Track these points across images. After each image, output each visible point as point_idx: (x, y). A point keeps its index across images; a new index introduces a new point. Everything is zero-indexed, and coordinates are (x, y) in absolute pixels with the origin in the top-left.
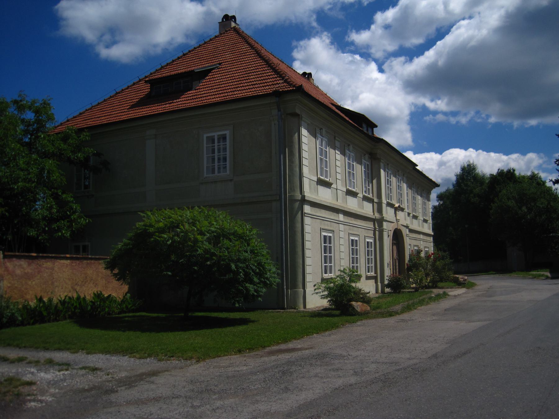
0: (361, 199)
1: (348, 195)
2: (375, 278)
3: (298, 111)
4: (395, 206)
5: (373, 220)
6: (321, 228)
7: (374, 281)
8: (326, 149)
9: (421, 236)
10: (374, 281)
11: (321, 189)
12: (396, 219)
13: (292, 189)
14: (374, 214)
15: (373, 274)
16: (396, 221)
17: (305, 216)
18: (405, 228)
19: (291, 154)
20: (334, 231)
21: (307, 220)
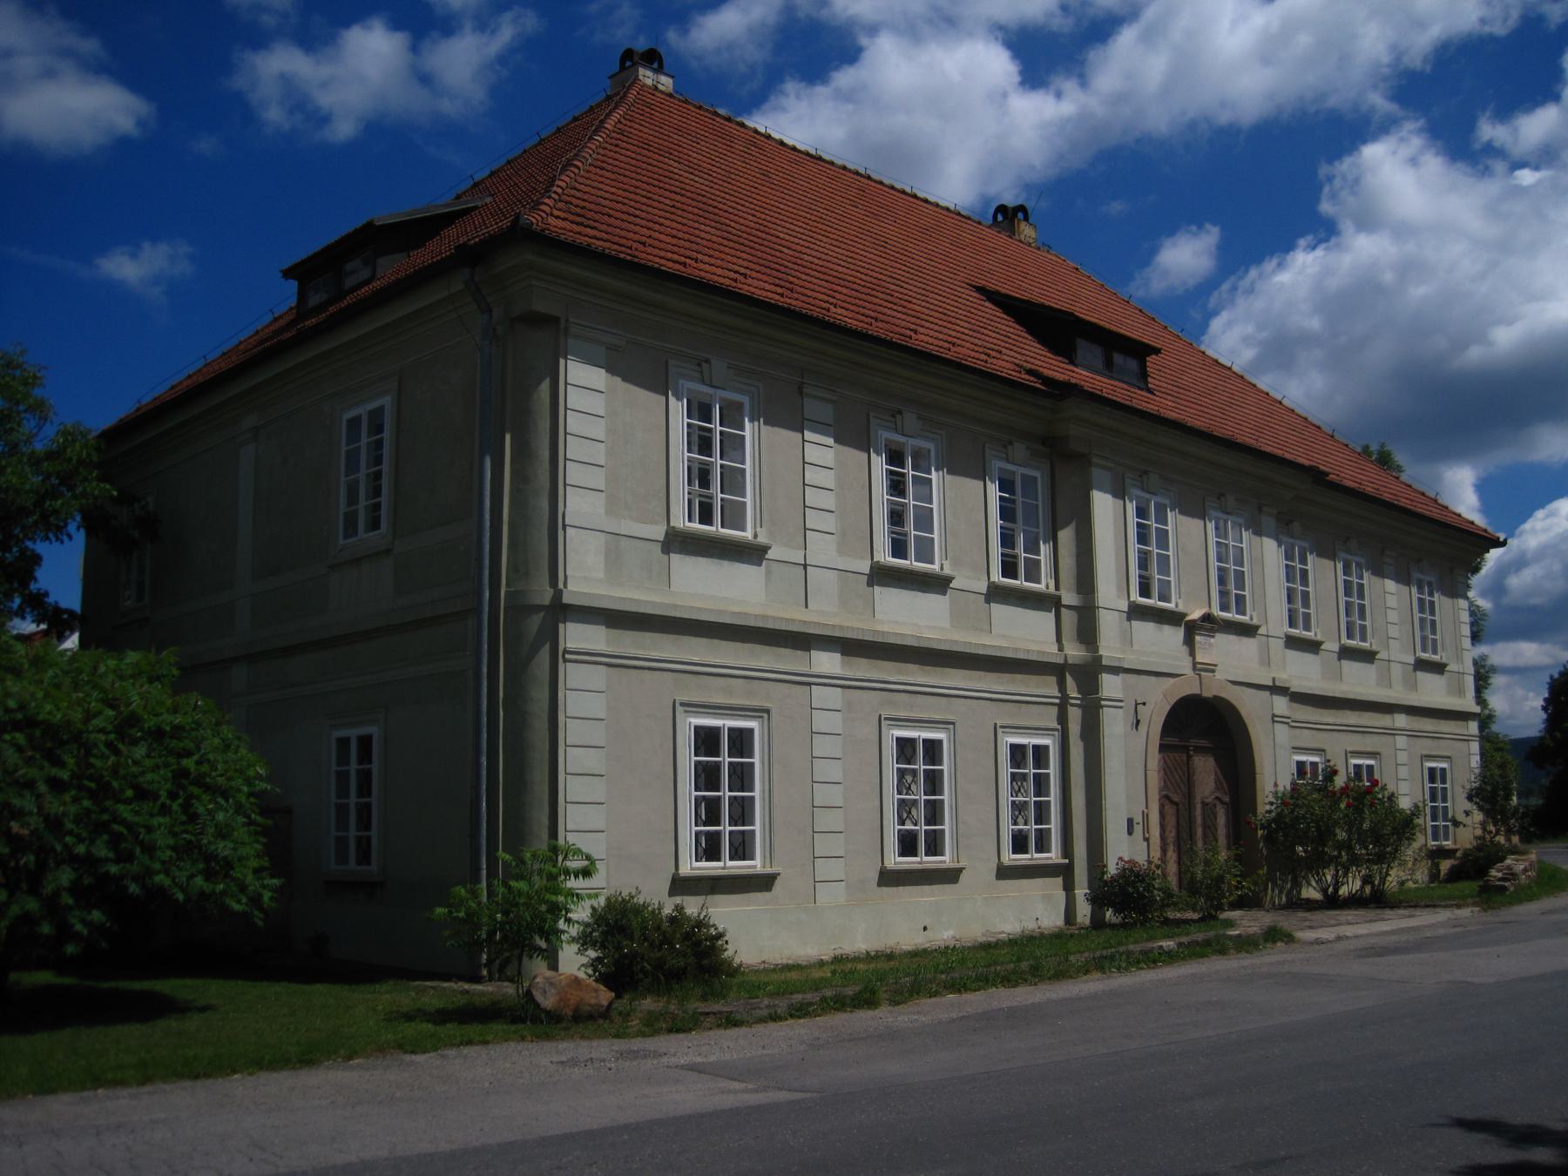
0: (658, 548)
1: (1422, 670)
2: (1065, 872)
3: (541, 306)
4: (1189, 618)
5: (1058, 670)
6: (1346, 751)
7: (1059, 880)
8: (1362, 578)
9: (1401, 720)
10: (1059, 880)
11: (1425, 678)
12: (1195, 664)
13: (520, 569)
14: (1061, 649)
15: (1054, 855)
16: (1194, 668)
17: (565, 661)
18: (1268, 693)
19: (523, 453)
20: (768, 711)
21: (573, 675)
